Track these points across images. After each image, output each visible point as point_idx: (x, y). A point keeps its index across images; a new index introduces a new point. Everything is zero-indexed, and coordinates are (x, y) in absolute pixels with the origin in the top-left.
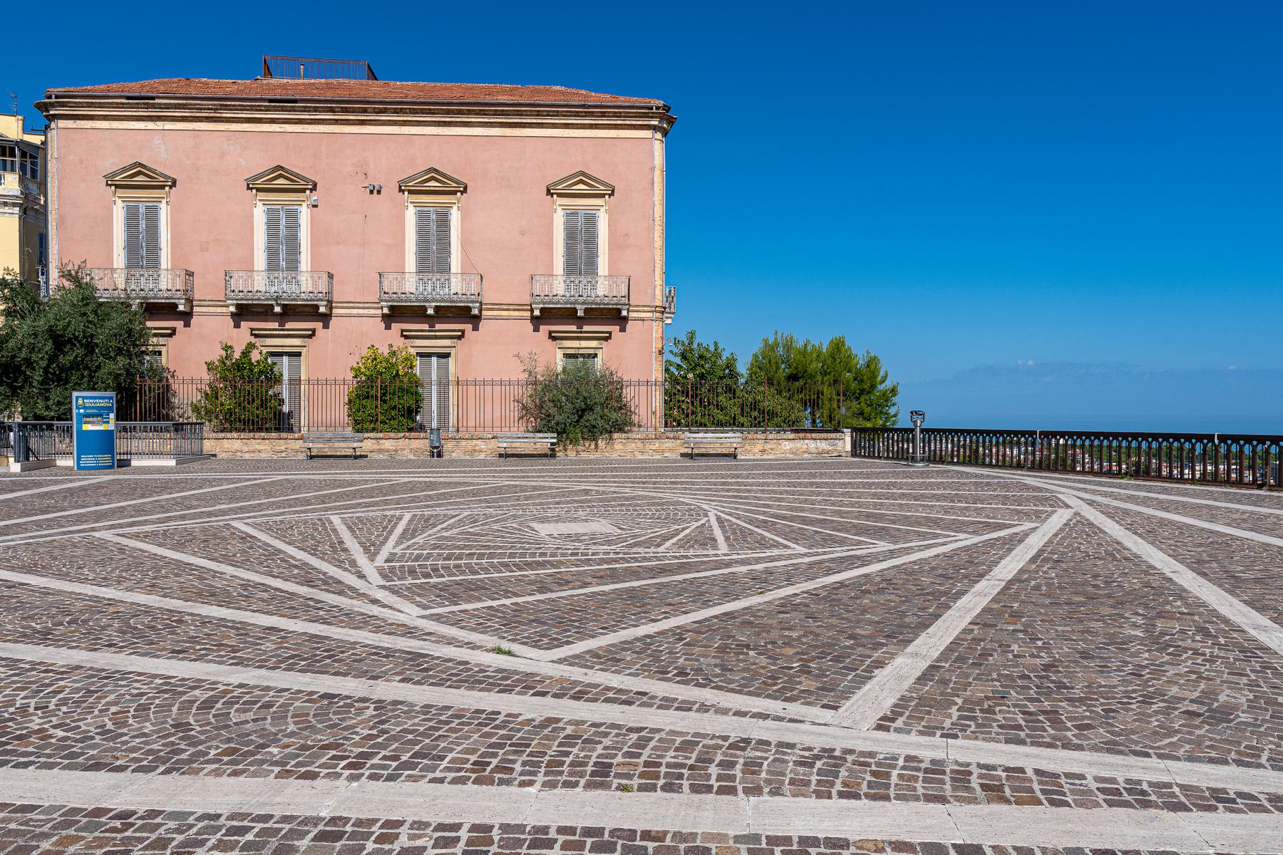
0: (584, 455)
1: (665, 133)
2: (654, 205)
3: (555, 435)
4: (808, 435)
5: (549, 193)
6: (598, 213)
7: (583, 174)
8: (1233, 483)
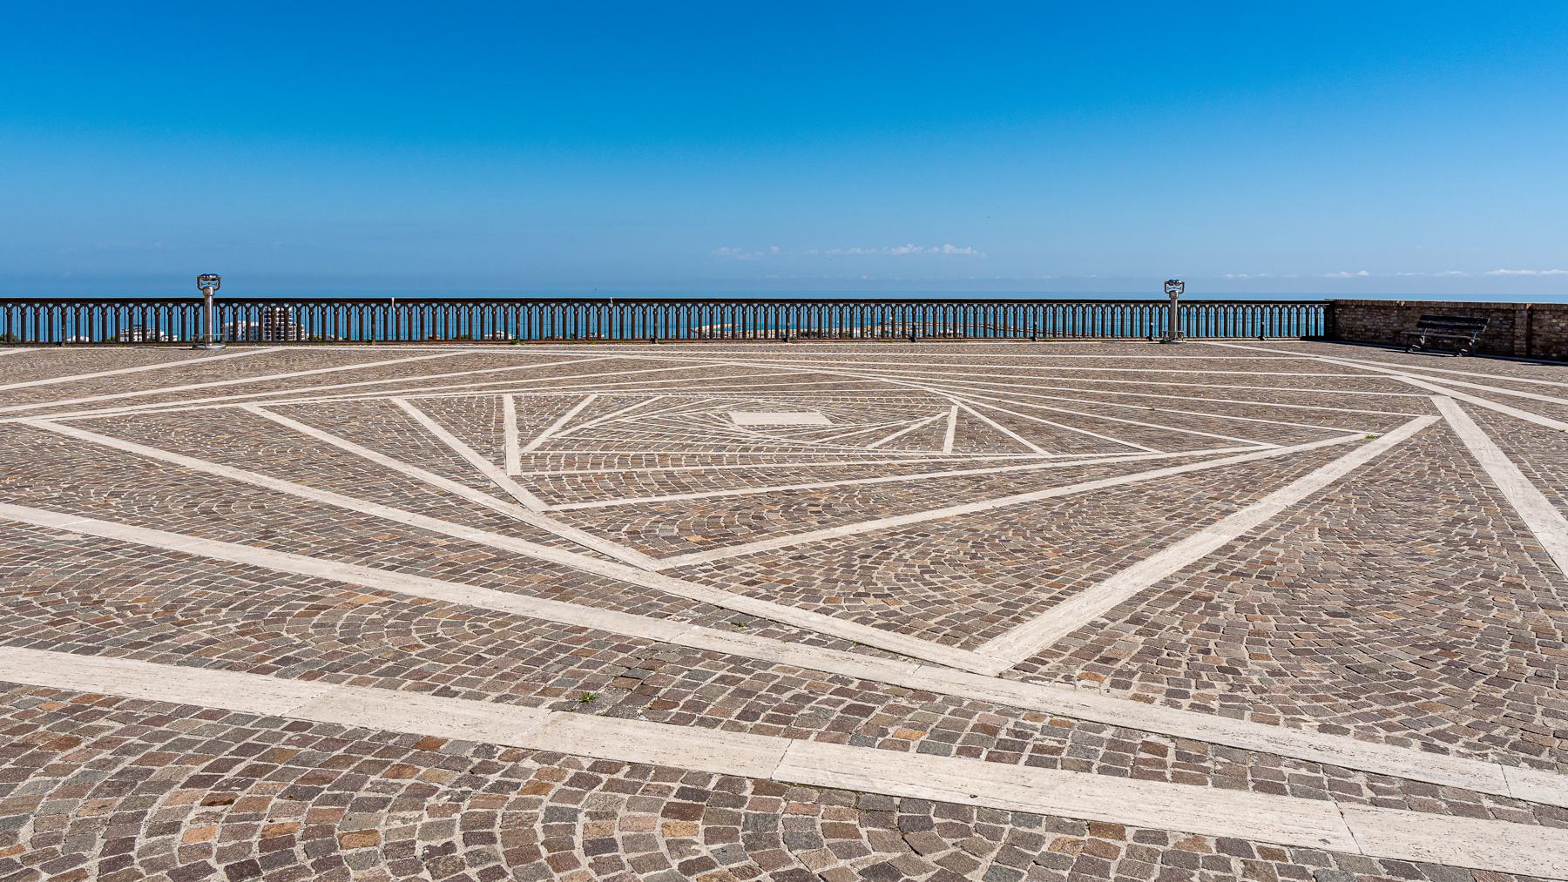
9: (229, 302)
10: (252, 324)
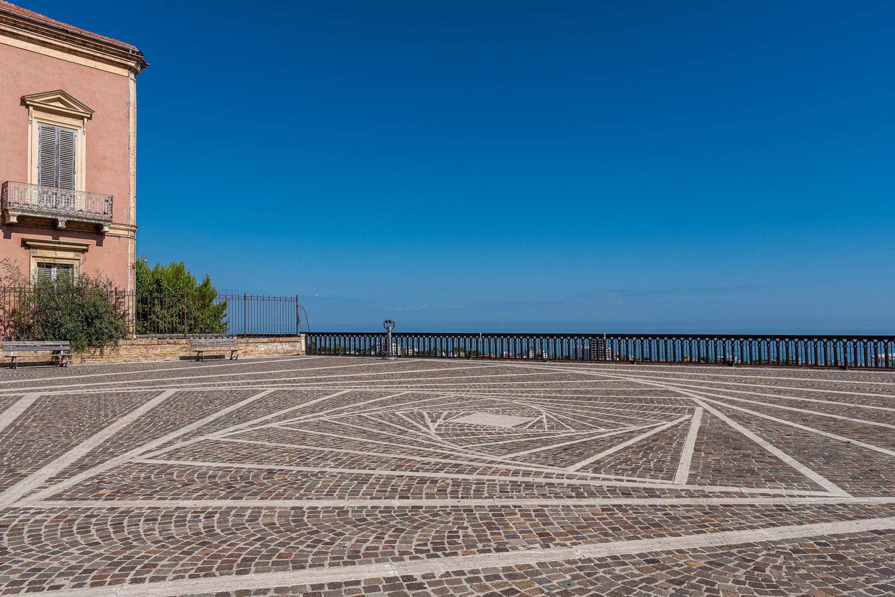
0: (89, 362)
1: (136, 73)
2: (129, 136)
3: (67, 343)
4: (277, 339)
5: (23, 102)
6: (75, 133)
7: (63, 93)
8: (531, 359)
9: (399, 335)
10: (586, 348)
